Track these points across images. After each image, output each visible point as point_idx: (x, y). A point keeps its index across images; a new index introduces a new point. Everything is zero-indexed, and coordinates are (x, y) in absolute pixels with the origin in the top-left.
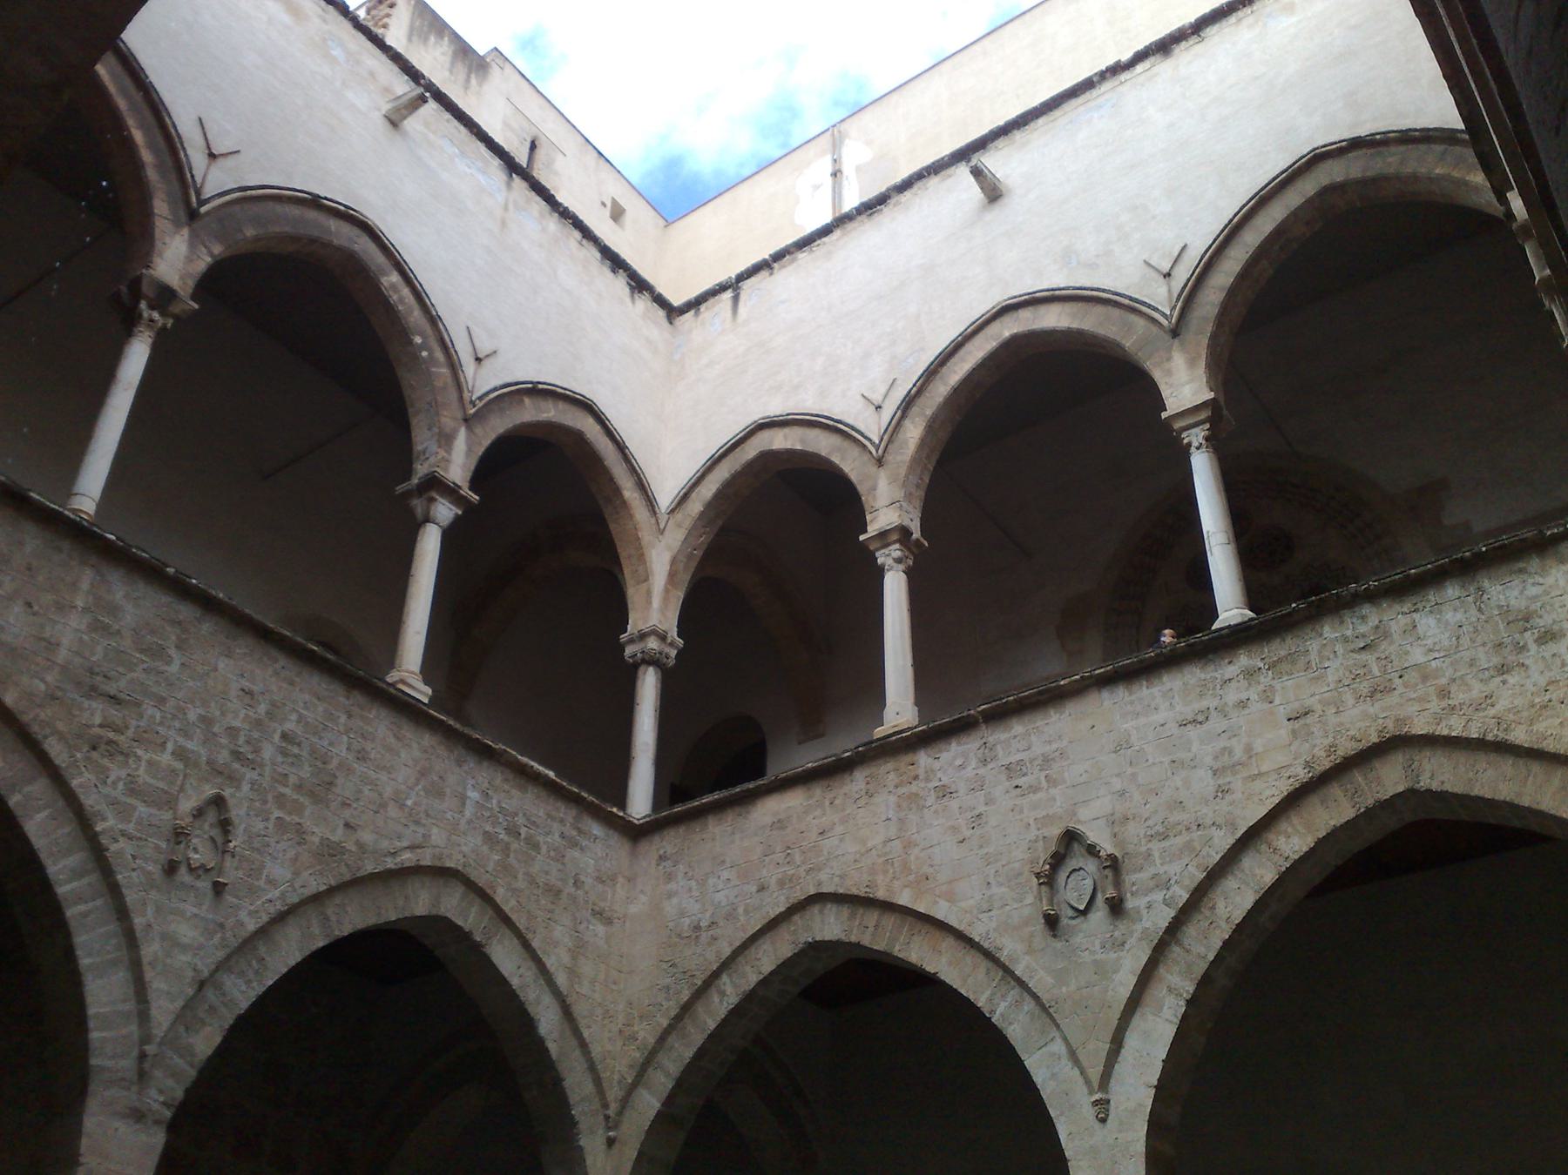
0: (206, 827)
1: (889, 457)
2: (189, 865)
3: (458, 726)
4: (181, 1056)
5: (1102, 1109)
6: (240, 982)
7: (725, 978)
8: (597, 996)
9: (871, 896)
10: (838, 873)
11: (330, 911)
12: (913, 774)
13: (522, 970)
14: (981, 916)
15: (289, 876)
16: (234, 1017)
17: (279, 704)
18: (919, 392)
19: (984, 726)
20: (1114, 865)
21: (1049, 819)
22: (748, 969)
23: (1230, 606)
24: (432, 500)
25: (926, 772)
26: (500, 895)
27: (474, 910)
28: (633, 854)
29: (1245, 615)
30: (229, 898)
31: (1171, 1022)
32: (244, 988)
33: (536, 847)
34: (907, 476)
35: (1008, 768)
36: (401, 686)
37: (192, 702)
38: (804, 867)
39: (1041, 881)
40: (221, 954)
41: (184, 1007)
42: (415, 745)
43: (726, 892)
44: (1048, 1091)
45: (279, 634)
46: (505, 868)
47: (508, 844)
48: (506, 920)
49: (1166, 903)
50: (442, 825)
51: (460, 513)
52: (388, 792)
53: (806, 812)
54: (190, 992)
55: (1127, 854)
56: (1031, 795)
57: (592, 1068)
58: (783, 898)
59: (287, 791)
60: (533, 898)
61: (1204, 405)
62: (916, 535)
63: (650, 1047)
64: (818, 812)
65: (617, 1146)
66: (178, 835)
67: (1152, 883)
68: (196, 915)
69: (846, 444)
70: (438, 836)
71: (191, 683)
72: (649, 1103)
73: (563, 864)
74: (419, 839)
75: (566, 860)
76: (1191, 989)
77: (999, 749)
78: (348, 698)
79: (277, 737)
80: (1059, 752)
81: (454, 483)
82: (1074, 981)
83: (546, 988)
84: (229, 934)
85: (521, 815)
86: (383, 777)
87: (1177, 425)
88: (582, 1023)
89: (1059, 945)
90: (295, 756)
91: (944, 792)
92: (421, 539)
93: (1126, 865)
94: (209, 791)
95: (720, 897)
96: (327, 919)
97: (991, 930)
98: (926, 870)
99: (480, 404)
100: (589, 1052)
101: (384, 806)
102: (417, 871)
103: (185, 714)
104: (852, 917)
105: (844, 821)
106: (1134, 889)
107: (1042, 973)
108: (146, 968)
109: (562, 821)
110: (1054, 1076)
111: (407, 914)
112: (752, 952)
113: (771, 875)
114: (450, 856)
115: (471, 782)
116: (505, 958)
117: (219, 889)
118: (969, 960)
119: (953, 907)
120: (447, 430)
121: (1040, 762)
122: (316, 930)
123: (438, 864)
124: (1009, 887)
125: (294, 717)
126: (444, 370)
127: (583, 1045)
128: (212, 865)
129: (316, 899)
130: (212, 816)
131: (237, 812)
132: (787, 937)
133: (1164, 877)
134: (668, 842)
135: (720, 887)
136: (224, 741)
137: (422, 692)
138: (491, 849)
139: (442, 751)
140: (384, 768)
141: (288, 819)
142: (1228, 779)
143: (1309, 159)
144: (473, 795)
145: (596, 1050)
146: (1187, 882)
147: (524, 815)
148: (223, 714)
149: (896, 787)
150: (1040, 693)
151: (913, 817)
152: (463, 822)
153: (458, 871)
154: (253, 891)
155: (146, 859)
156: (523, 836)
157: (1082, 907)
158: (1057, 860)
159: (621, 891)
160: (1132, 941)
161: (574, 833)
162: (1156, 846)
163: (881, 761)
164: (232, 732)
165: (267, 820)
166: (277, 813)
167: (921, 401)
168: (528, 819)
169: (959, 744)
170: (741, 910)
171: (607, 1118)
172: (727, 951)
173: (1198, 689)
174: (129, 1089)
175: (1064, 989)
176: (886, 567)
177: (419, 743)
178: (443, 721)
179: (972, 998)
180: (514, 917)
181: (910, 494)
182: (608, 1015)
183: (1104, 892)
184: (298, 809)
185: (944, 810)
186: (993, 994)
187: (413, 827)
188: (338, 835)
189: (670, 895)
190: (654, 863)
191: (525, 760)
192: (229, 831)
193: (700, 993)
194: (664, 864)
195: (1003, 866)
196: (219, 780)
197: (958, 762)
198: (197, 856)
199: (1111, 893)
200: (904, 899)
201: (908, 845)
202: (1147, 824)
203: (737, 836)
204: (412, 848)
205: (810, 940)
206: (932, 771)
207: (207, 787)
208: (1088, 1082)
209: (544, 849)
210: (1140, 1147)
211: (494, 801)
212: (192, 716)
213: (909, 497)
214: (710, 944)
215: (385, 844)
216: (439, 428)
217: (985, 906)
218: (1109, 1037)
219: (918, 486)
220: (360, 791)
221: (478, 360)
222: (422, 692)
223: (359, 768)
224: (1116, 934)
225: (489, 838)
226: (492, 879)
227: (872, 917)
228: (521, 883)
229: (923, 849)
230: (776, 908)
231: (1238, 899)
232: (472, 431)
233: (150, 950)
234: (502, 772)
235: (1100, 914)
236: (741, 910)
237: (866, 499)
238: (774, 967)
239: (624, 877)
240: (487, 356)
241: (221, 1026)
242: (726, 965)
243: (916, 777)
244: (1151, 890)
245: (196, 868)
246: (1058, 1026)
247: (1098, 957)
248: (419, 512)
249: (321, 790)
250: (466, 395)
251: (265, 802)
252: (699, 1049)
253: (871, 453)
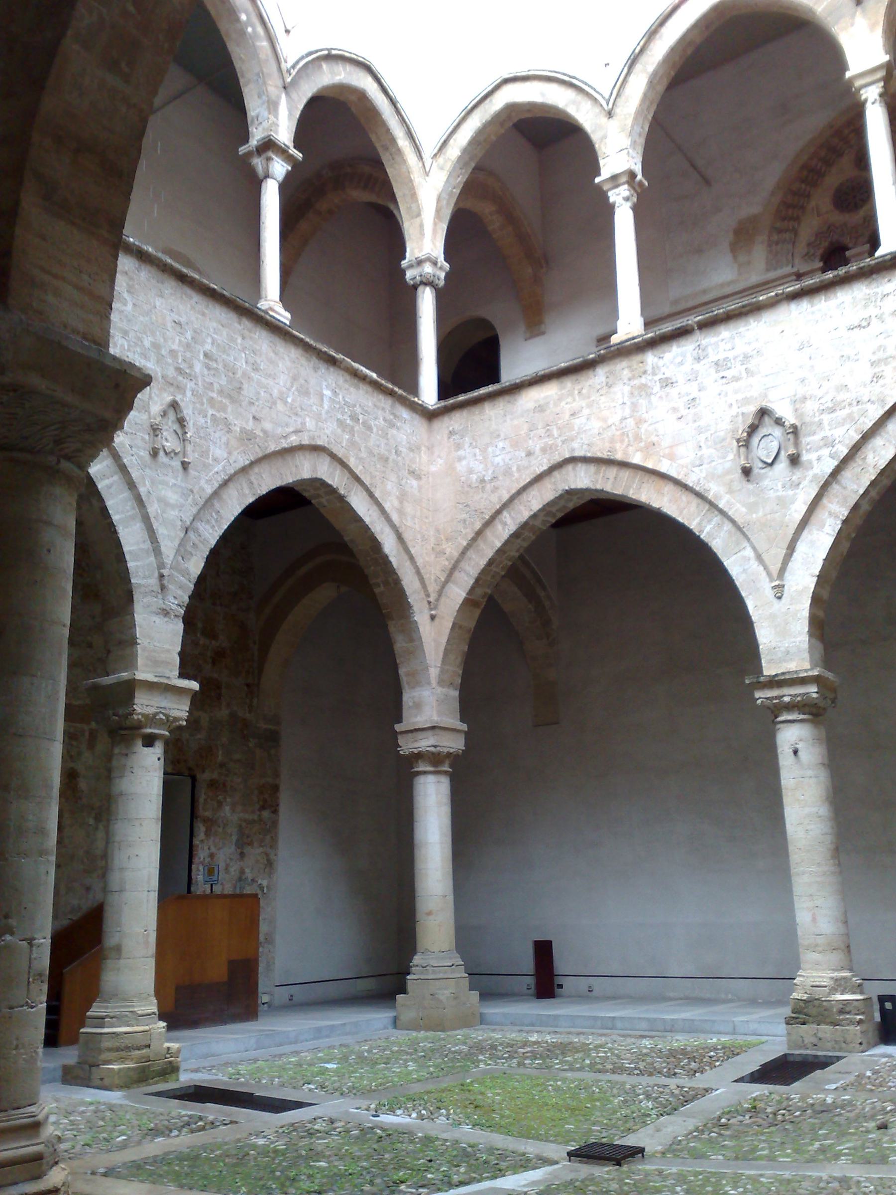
0: (170, 423)
1: (618, 110)
2: (165, 451)
3: (312, 342)
4: (183, 576)
5: (779, 592)
6: (208, 527)
7: (505, 514)
8: (417, 527)
9: (612, 458)
10: (586, 442)
11: (253, 478)
12: (642, 370)
13: (370, 512)
14: (694, 469)
15: (225, 455)
16: (208, 550)
17: (198, 331)
18: (642, 51)
19: (698, 332)
20: (795, 431)
21: (746, 401)
22: (522, 508)
24: (269, 159)
25: (653, 368)
26: (352, 462)
27: (338, 472)
28: (430, 431)
30: (192, 472)
31: (830, 535)
32: (211, 531)
33: (369, 428)
34: (632, 126)
35: (717, 364)
36: (271, 313)
37: (145, 333)
38: (560, 439)
39: (740, 444)
40: (194, 510)
41: (179, 545)
42: (287, 358)
43: (502, 456)
44: (741, 580)
45: (191, 277)
46: (352, 443)
47: (353, 428)
48: (357, 479)
49: (832, 456)
50: (311, 415)
51: (290, 168)
52: (275, 393)
53: (560, 399)
54: (182, 535)
55: (804, 423)
56: (734, 383)
57: (418, 572)
58: (545, 460)
59: (214, 395)
60: (372, 463)
62: (640, 177)
63: (455, 559)
64: (569, 400)
65: (437, 620)
66: (154, 430)
67: (822, 443)
68: (175, 484)
69: (580, 98)
70: (310, 424)
71: (141, 318)
72: (458, 593)
73: (387, 439)
74: (299, 427)
75: (389, 436)
76: (846, 513)
77: (710, 350)
78: (240, 324)
79: (202, 357)
80: (756, 351)
81: (284, 144)
82: (761, 510)
83: (386, 523)
84: (197, 496)
85: (358, 406)
86: (271, 382)
87: (858, 83)
88: (410, 544)
89: (750, 486)
90: (214, 369)
91: (667, 383)
92: (265, 193)
93: (802, 432)
94: (169, 398)
95: (498, 460)
96: (252, 483)
97: (702, 479)
98: (654, 439)
99: (294, 72)
100: (416, 563)
101: (274, 403)
102: (301, 448)
103: (142, 342)
104: (597, 473)
105: (589, 406)
106: (808, 447)
107: (738, 505)
108: (153, 520)
109: (383, 409)
110: (745, 571)
111: (299, 478)
112: (524, 496)
113: (536, 445)
114: (319, 437)
115: (325, 383)
116: (359, 504)
117: (185, 465)
118: (684, 498)
119: (673, 464)
120: (273, 97)
121: (741, 358)
122: (247, 491)
123: (313, 443)
124: (715, 449)
125: (209, 340)
126: (265, 44)
127: (412, 558)
128: (179, 450)
129: (244, 470)
130: (172, 415)
131: (187, 412)
132: (549, 486)
133: (830, 439)
134: (456, 421)
135: (498, 453)
136: (170, 361)
137: (284, 316)
138: (343, 431)
139: (303, 361)
140: (270, 376)
141: (218, 415)
142: (880, 369)
144: (327, 393)
145: (420, 562)
146: (847, 442)
147: (360, 405)
148: (165, 340)
149: (630, 379)
150: (743, 307)
151: (643, 402)
152: (323, 412)
153: (325, 447)
154: (206, 466)
155: (138, 448)
156: (361, 421)
158: (753, 429)
159: (424, 457)
160: (805, 483)
161: (392, 417)
162: (826, 418)
163: (617, 361)
164: (173, 353)
165: (206, 416)
166: (211, 412)
167: (644, 59)
168: (363, 409)
169: (678, 347)
170: (514, 469)
171: (429, 603)
172: (506, 497)
173: (863, 302)
174: (156, 597)
175: (754, 516)
177: (289, 356)
178: (302, 339)
179: (686, 523)
180: (362, 477)
181: (635, 142)
182: (424, 539)
183: (786, 451)
184: (223, 409)
185: (667, 396)
186: (702, 520)
187: (294, 418)
188: (250, 425)
189: (460, 459)
190: (445, 437)
191: (356, 365)
192: (185, 426)
193: (488, 523)
194: (454, 437)
195: (711, 434)
196: (172, 389)
197: (679, 359)
198: (168, 444)
199: (792, 450)
200: (637, 459)
201: (639, 422)
202: (821, 401)
203: (508, 417)
204: (296, 432)
205: (567, 488)
206: (658, 367)
207: (165, 395)
208: (769, 574)
209: (375, 430)
210: (806, 613)
211: (341, 397)
212: (147, 343)
213: (634, 144)
214: (492, 492)
215: (279, 431)
216: (268, 96)
217: (697, 463)
218: (786, 545)
219: (640, 135)
220: (259, 393)
221: (287, 31)
222: (284, 316)
223: (255, 376)
224: (794, 478)
225: (341, 423)
226: (346, 452)
227: (612, 472)
228: (364, 454)
229: (651, 424)
230: (541, 467)
231: (883, 452)
232: (290, 97)
233: (153, 509)
234: (343, 375)
235: (783, 465)
236: (514, 469)
237: (599, 146)
238: (541, 506)
239: (425, 446)
241: (201, 556)
242: (505, 505)
243: (645, 372)
244: (820, 448)
245: (170, 453)
246: (748, 539)
247: (780, 494)
248: (260, 170)
249: (234, 393)
250: (283, 65)
251: (202, 404)
252: (490, 559)
253: (601, 105)
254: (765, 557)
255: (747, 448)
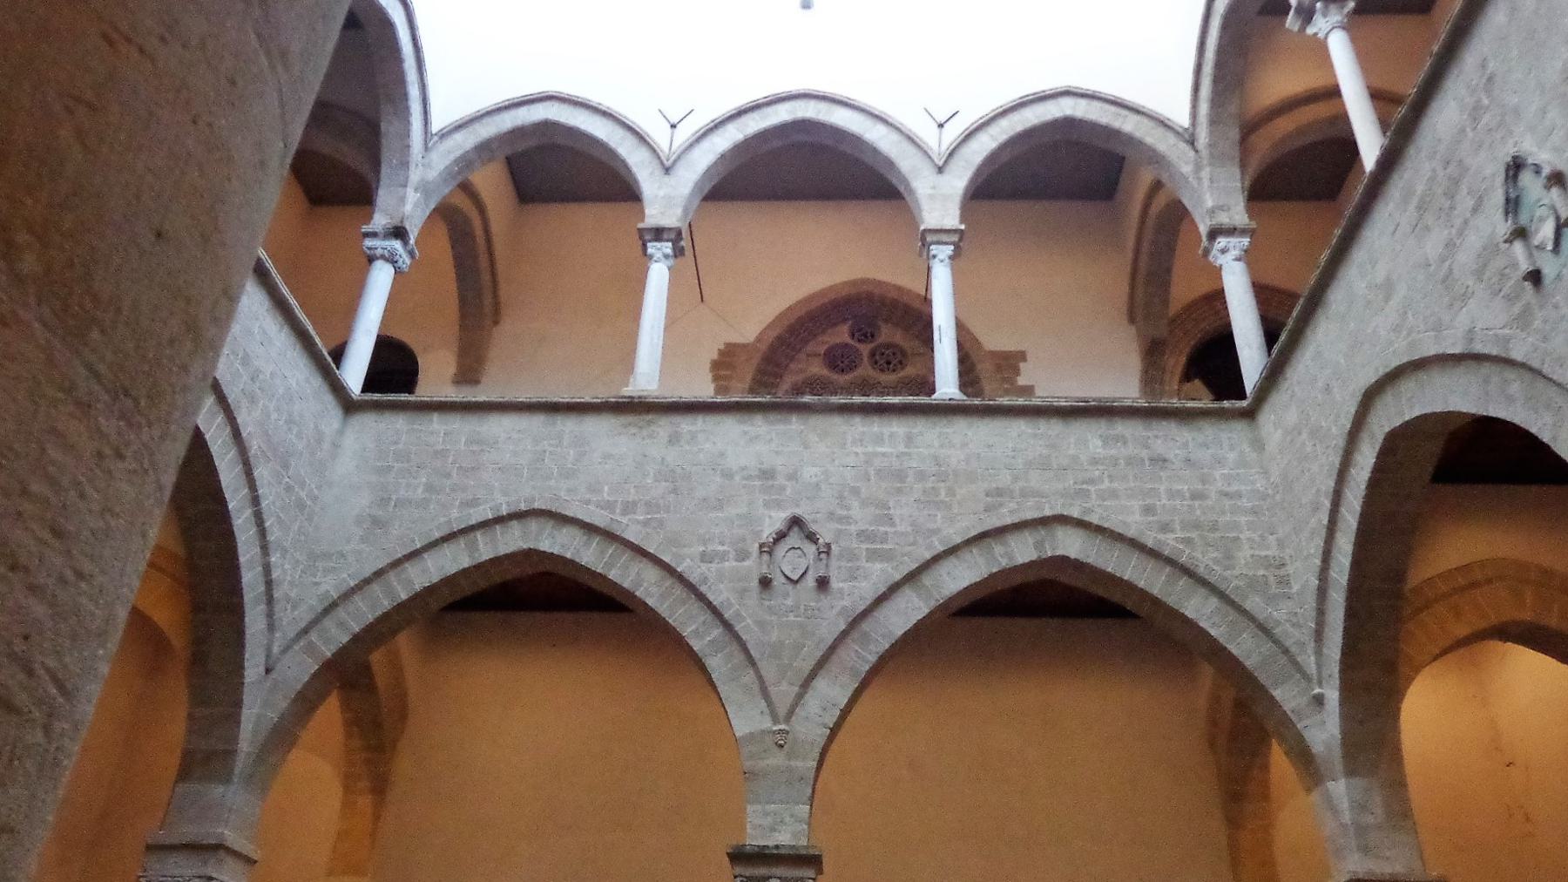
23: (947, 386)
29: (219, 425)
51: (1249, 240)
61: (955, 231)
143: (1078, 406)
157: (795, 577)
176: (655, 258)
240: (675, 162)
254: (772, 690)
255: (771, 556)
